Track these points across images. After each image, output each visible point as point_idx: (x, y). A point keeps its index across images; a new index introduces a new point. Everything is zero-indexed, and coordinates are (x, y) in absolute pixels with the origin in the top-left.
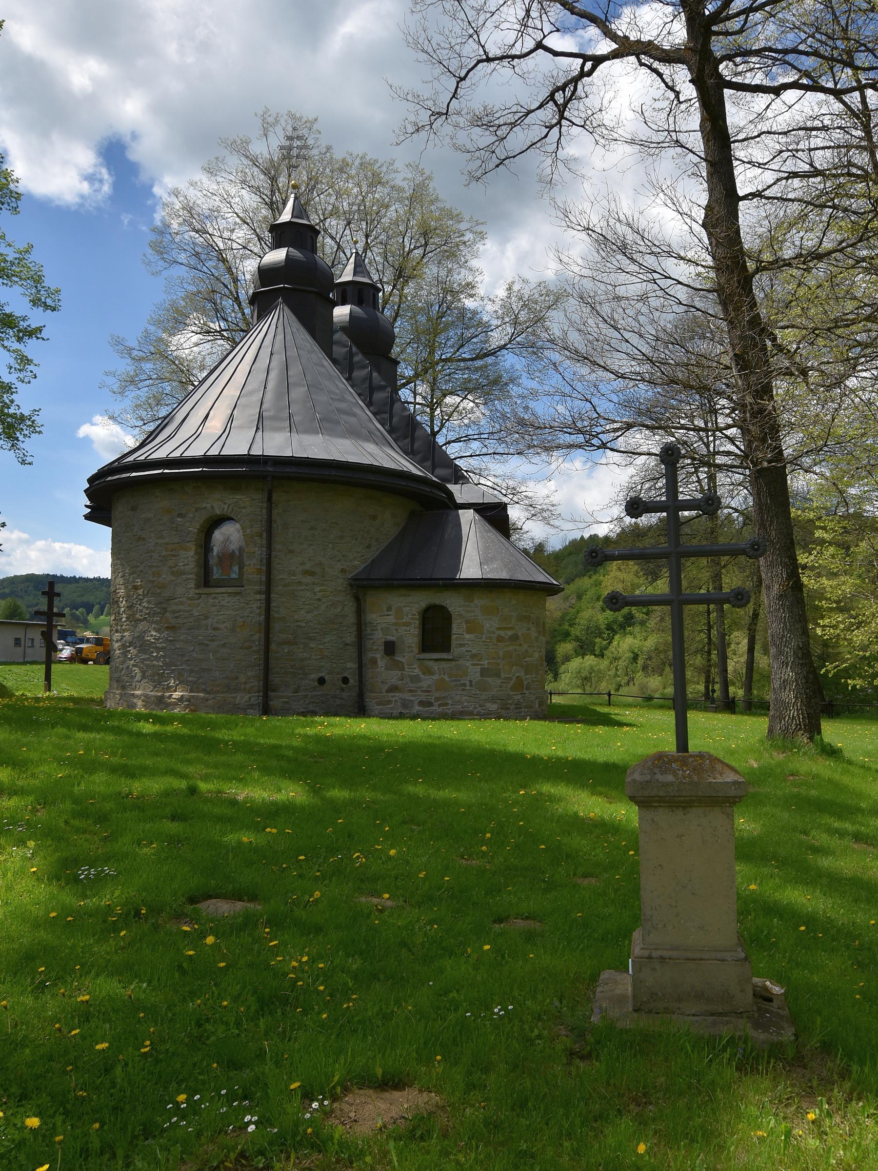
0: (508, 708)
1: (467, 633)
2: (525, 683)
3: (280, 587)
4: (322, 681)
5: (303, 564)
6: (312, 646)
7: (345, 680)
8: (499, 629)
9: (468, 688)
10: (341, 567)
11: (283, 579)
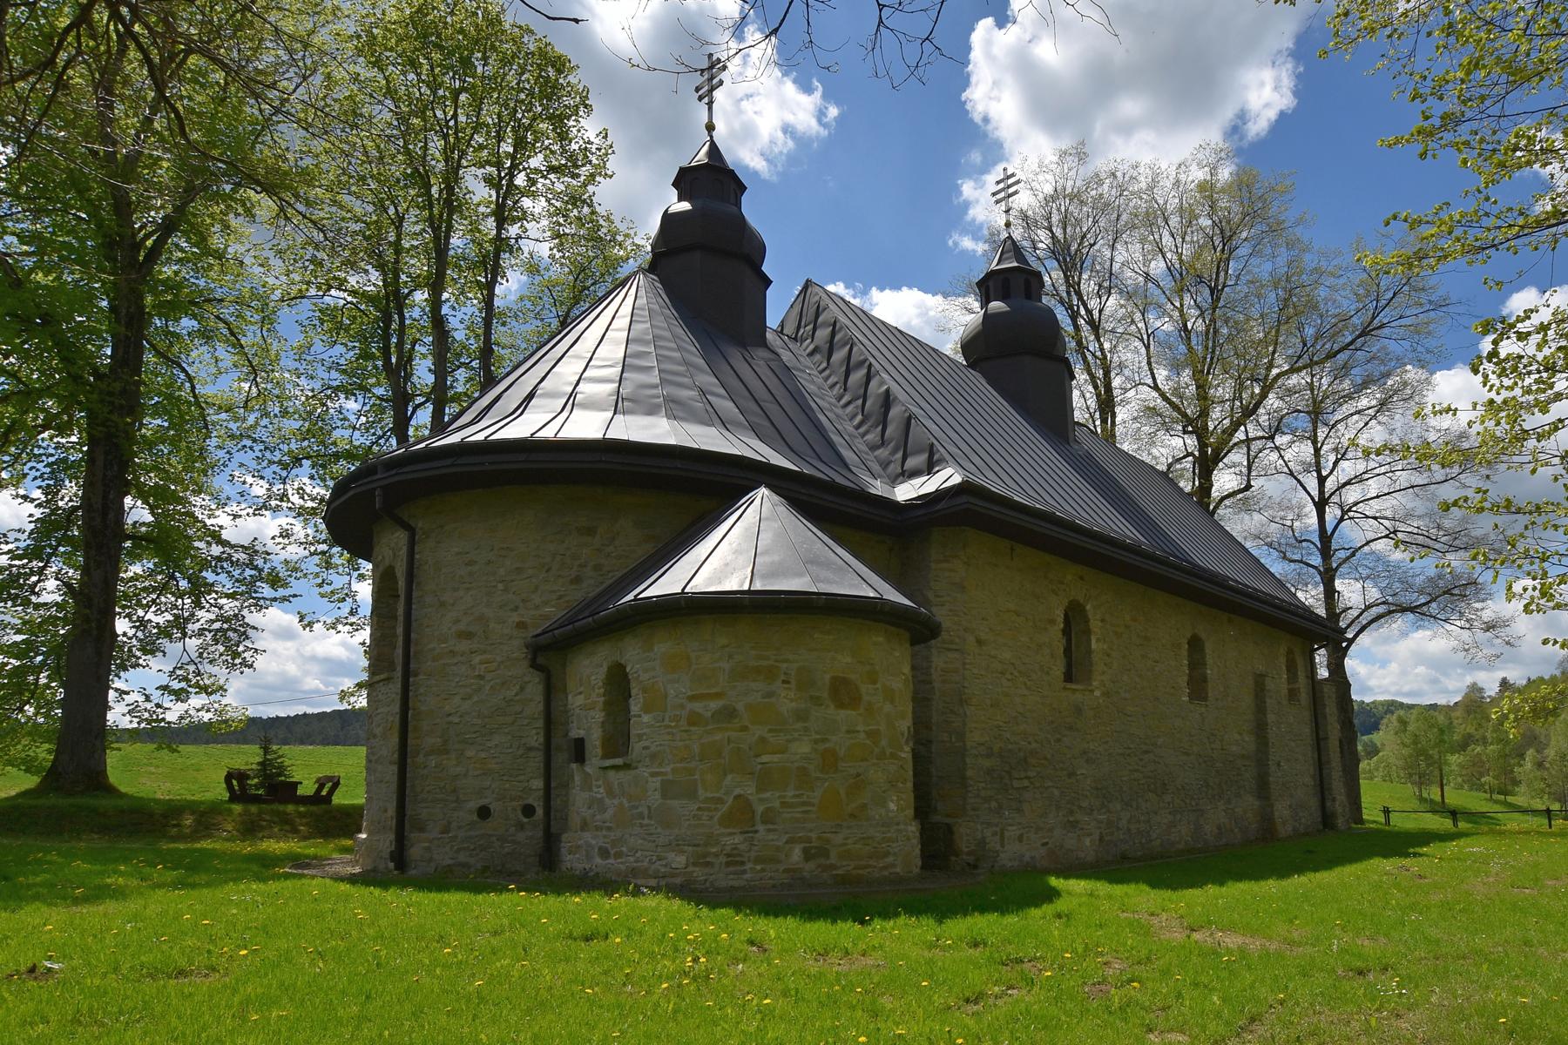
0: (708, 864)
1: (645, 713)
2: (760, 809)
3: (429, 663)
4: (484, 813)
5: (457, 621)
6: (469, 753)
7: (528, 810)
8: (692, 698)
9: (646, 821)
10: (517, 620)
11: (434, 649)
